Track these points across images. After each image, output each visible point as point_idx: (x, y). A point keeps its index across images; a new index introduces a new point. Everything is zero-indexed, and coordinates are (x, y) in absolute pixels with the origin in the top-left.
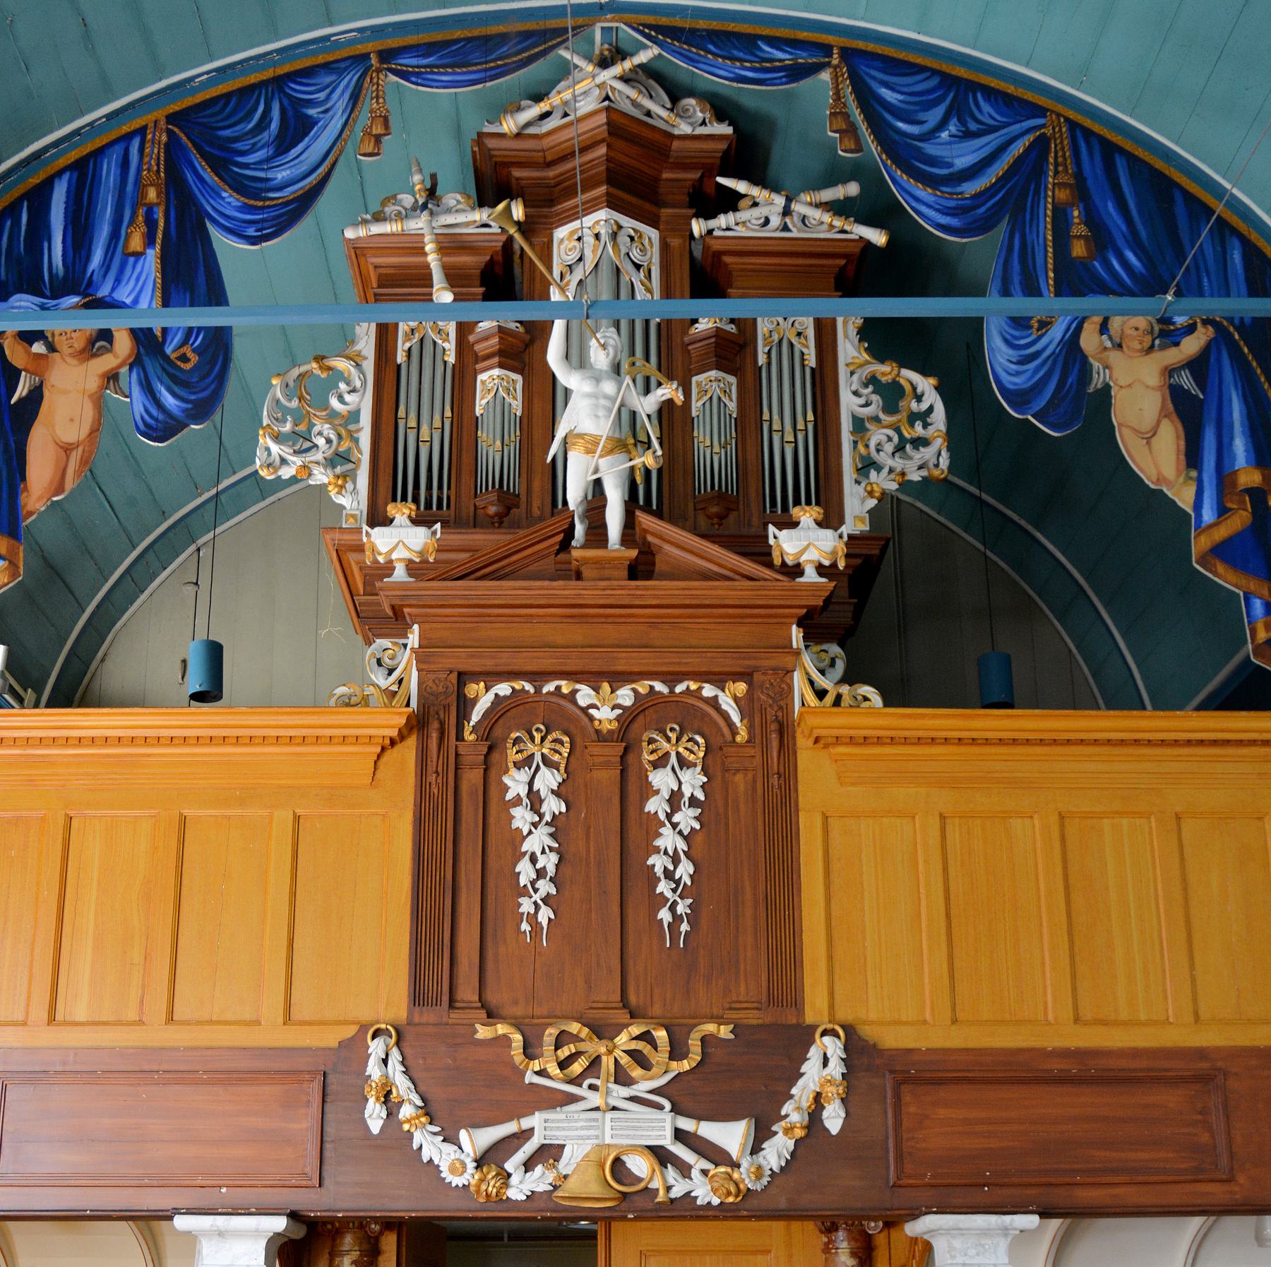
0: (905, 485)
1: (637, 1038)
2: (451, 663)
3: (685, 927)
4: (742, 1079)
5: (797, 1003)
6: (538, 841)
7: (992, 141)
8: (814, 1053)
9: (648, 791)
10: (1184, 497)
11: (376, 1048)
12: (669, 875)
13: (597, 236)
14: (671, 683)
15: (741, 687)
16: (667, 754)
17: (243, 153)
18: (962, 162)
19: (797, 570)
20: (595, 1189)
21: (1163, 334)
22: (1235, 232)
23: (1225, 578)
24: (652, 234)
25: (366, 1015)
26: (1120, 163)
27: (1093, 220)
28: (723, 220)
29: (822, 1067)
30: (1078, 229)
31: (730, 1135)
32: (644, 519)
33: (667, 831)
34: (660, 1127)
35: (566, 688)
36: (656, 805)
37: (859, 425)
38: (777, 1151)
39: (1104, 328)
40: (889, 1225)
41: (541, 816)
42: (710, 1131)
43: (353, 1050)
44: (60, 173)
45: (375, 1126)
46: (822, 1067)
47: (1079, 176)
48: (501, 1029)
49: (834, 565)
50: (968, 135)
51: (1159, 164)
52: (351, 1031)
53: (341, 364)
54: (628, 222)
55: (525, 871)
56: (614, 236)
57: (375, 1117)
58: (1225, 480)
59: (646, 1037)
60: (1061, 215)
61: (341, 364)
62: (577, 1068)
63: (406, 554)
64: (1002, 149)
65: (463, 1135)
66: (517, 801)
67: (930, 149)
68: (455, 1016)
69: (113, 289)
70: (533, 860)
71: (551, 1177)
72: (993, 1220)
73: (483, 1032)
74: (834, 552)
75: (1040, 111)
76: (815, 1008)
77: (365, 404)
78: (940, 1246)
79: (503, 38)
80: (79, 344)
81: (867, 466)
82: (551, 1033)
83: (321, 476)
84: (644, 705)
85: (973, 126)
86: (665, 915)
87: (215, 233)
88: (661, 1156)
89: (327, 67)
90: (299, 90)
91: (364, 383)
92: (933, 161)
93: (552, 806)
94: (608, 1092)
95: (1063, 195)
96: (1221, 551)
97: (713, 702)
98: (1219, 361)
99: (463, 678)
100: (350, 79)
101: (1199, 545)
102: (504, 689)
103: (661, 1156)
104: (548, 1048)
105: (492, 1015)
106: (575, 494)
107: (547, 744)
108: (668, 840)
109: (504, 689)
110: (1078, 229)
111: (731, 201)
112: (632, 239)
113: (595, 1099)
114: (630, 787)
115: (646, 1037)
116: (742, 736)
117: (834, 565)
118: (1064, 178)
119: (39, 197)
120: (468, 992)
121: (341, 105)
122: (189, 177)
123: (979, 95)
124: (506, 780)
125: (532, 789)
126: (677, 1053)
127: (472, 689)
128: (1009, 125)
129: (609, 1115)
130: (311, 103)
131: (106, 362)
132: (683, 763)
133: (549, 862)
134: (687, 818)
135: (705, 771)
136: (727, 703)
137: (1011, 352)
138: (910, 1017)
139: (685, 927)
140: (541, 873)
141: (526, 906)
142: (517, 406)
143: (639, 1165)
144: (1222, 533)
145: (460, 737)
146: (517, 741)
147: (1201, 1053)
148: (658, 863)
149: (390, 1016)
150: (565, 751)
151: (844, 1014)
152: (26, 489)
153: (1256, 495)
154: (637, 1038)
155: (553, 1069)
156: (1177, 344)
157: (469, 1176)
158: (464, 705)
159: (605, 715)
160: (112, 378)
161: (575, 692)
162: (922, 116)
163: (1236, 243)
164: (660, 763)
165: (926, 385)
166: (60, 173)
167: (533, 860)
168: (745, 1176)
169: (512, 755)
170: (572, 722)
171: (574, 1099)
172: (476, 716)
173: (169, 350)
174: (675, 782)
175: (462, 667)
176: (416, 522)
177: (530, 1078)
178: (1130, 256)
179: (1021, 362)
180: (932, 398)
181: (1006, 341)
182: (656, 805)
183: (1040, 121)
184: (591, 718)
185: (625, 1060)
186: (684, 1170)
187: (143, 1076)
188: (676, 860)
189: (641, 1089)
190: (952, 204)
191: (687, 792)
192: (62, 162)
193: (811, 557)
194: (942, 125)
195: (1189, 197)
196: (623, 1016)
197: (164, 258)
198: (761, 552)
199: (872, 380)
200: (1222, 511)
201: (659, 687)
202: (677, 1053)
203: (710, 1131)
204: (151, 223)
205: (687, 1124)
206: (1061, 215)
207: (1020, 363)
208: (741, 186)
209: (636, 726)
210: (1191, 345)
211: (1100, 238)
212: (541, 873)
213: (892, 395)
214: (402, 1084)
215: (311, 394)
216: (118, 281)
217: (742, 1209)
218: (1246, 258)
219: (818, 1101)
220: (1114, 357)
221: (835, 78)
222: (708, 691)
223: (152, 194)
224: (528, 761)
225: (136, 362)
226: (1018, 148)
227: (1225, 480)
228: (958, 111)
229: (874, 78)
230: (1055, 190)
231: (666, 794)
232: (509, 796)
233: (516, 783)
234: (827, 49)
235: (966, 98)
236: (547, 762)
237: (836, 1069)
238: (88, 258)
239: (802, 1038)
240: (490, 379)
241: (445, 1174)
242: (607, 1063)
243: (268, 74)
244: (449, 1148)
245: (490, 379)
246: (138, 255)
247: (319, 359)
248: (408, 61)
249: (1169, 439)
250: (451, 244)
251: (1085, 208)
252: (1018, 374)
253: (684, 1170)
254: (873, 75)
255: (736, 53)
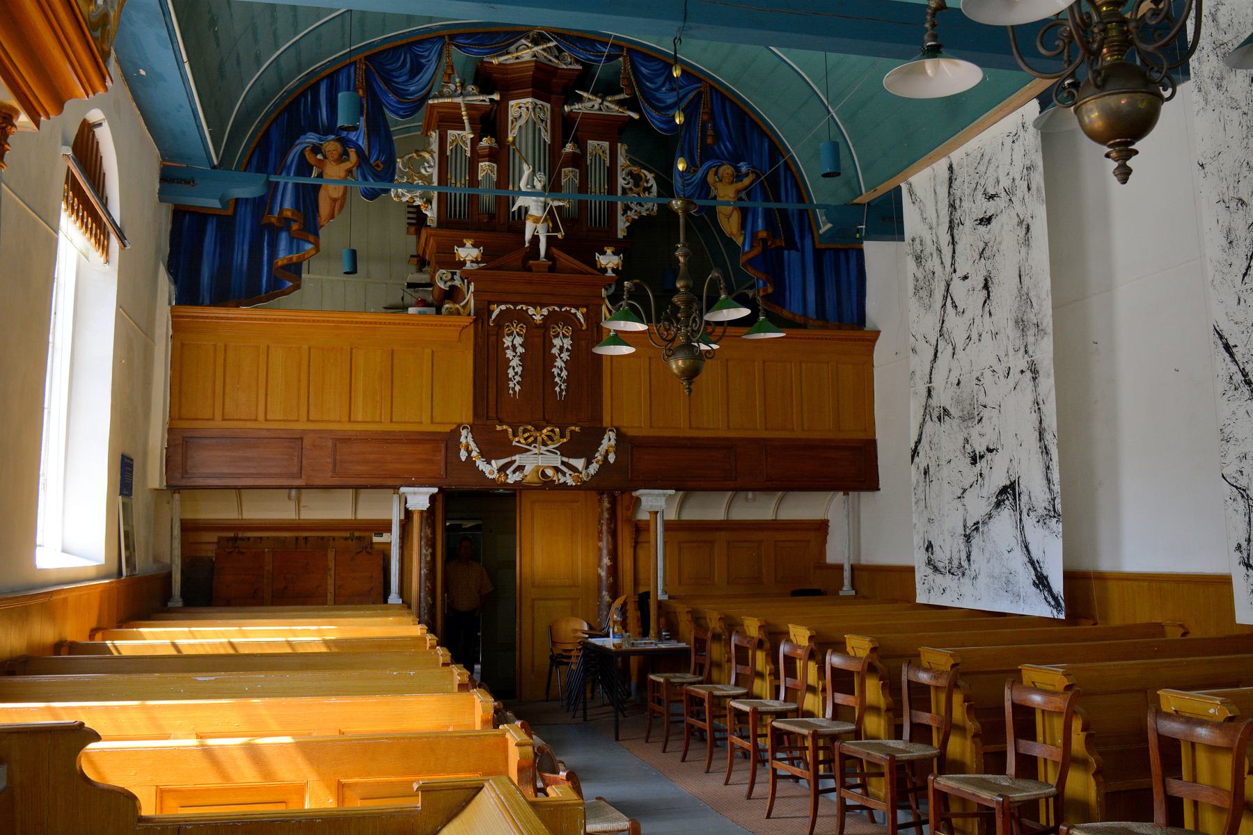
0: (641, 217)
4: (582, 445)
5: (601, 421)
6: (515, 362)
7: (682, 92)
8: (606, 437)
10: (739, 241)
11: (464, 433)
14: (561, 307)
15: (585, 310)
18: (670, 101)
20: (536, 480)
21: (737, 176)
22: (767, 135)
23: (750, 272)
24: (548, 105)
25: (459, 421)
26: (727, 104)
27: (715, 128)
29: (608, 441)
30: (710, 132)
31: (579, 463)
32: (554, 250)
34: (557, 460)
36: (555, 351)
37: (624, 191)
38: (593, 468)
40: (622, 493)
42: (573, 462)
43: (455, 434)
44: (322, 79)
45: (463, 459)
46: (608, 441)
47: (712, 109)
51: (742, 106)
52: (454, 426)
53: (427, 155)
54: (539, 102)
55: (511, 373)
56: (534, 109)
57: (463, 455)
58: (754, 235)
59: (552, 431)
61: (427, 155)
62: (530, 440)
65: (493, 462)
66: (508, 348)
67: (658, 95)
68: (489, 422)
72: (661, 491)
73: (499, 428)
75: (700, 80)
76: (606, 421)
77: (435, 172)
78: (643, 499)
79: (498, 33)
81: (627, 208)
82: (521, 429)
83: (418, 202)
86: (557, 389)
88: (557, 469)
89: (428, 40)
90: (418, 50)
92: (659, 100)
93: (520, 350)
95: (705, 117)
96: (750, 262)
99: (490, 303)
100: (437, 47)
101: (743, 259)
102: (503, 307)
103: (557, 469)
105: (501, 423)
106: (528, 236)
108: (559, 363)
109: (503, 307)
110: (710, 132)
111: (580, 99)
113: (536, 451)
115: (552, 431)
116: (584, 327)
119: (315, 88)
120: (492, 414)
121: (434, 59)
125: (514, 343)
126: (562, 436)
130: (422, 57)
131: (347, 165)
133: (519, 369)
134: (565, 356)
136: (579, 315)
138: (637, 422)
141: (511, 385)
142: (495, 177)
143: (550, 472)
144: (750, 255)
147: (728, 439)
148: (556, 371)
151: (616, 424)
153: (764, 240)
157: (495, 476)
159: (538, 318)
160: (349, 172)
164: (557, 336)
165: (650, 176)
166: (322, 79)
168: (584, 476)
170: (524, 318)
171: (529, 450)
174: (561, 343)
180: (652, 182)
182: (555, 351)
186: (564, 474)
187: (386, 441)
189: (551, 447)
192: (324, 74)
194: (663, 85)
195: (752, 121)
196: (544, 423)
197: (367, 121)
198: (593, 263)
199: (630, 174)
200: (752, 247)
202: (562, 436)
203: (573, 462)
205: (565, 459)
211: (718, 137)
213: (637, 179)
214: (473, 445)
215: (415, 166)
217: (583, 487)
218: (770, 146)
219: (607, 452)
220: (719, 185)
222: (573, 311)
224: (511, 334)
225: (359, 166)
226: (691, 96)
227: (754, 235)
233: (507, 341)
234: (621, 48)
237: (613, 442)
239: (601, 432)
240: (484, 166)
242: (539, 439)
243: (404, 41)
245: (484, 166)
247: (417, 151)
249: (735, 218)
250: (470, 107)
253: (564, 474)
254: (638, 60)
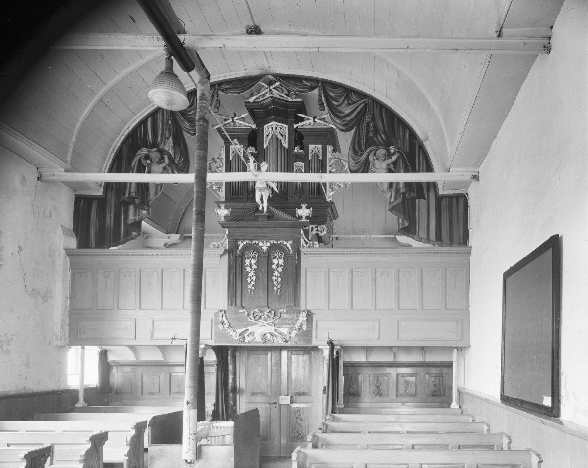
1: (268, 312)
2: (234, 238)
3: (279, 291)
5: (299, 306)
8: (301, 315)
9: (273, 264)
12: (276, 280)
13: (272, 128)
16: (276, 256)
17: (189, 112)
18: (347, 112)
19: (301, 218)
24: (286, 126)
27: (375, 127)
28: (301, 124)
30: (372, 129)
33: (276, 272)
34: (271, 329)
35: (257, 242)
36: (274, 267)
39: (375, 154)
41: (252, 269)
42: (281, 330)
48: (244, 310)
49: (309, 216)
50: (349, 104)
60: (368, 125)
62: (257, 318)
63: (224, 215)
64: (357, 108)
67: (340, 109)
69: (163, 147)
70: (251, 278)
71: (253, 338)
74: (309, 214)
76: (302, 308)
80: (157, 160)
82: (252, 312)
84: (273, 246)
85: (350, 102)
86: (275, 288)
87: (184, 132)
88: (272, 334)
91: (223, 165)
92: (341, 112)
94: (263, 322)
95: (369, 120)
97: (286, 245)
98: (400, 162)
103: (272, 334)
104: (252, 314)
107: (253, 254)
108: (276, 273)
109: (245, 243)
110: (372, 129)
111: (302, 120)
112: (281, 128)
113: (261, 324)
114: (269, 263)
115: (270, 312)
117: (309, 216)
118: (371, 116)
122: (177, 118)
123: (352, 93)
124: (245, 261)
125: (251, 263)
127: (239, 243)
128: (358, 101)
129: (263, 327)
132: (279, 258)
134: (280, 269)
135: (284, 259)
136: (288, 245)
137: (354, 161)
139: (279, 291)
140: (252, 280)
141: (249, 287)
145: (236, 253)
146: (248, 253)
148: (274, 278)
149: (224, 309)
150: (257, 256)
151: (308, 309)
152: (150, 195)
153: (404, 194)
154: (268, 312)
155: (253, 318)
156: (391, 158)
158: (237, 246)
161: (259, 243)
162: (339, 100)
163: (408, 131)
164: (275, 258)
167: (251, 278)
169: (247, 256)
170: (257, 249)
171: (256, 324)
172: (240, 248)
173: (176, 162)
174: (278, 262)
175: (236, 238)
176: (226, 208)
177: (249, 320)
178: (383, 136)
179: (355, 164)
181: (352, 158)
183: (366, 100)
184: (262, 249)
185: (266, 317)
186: (276, 337)
188: (278, 278)
189: (269, 322)
190: (344, 123)
191: (280, 263)
193: (304, 215)
194: (343, 102)
198: (294, 214)
200: (396, 198)
201: (275, 242)
204: (170, 130)
206: (368, 125)
207: (355, 164)
208: (303, 116)
209: (271, 251)
210: (394, 158)
211: (376, 131)
212: (252, 280)
216: (164, 145)
218: (409, 135)
219: (301, 325)
220: (377, 162)
221: (320, 90)
223: (170, 122)
226: (360, 108)
228: (348, 98)
229: (329, 89)
230: (368, 119)
231: (276, 264)
232: (246, 265)
233: (247, 262)
235: (349, 95)
236: (253, 258)
238: (157, 140)
241: (234, 337)
244: (234, 333)
246: (168, 138)
248: (224, 86)
251: (374, 123)
252: (354, 167)
254: (328, 88)
255: (298, 84)
